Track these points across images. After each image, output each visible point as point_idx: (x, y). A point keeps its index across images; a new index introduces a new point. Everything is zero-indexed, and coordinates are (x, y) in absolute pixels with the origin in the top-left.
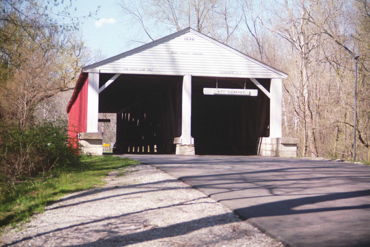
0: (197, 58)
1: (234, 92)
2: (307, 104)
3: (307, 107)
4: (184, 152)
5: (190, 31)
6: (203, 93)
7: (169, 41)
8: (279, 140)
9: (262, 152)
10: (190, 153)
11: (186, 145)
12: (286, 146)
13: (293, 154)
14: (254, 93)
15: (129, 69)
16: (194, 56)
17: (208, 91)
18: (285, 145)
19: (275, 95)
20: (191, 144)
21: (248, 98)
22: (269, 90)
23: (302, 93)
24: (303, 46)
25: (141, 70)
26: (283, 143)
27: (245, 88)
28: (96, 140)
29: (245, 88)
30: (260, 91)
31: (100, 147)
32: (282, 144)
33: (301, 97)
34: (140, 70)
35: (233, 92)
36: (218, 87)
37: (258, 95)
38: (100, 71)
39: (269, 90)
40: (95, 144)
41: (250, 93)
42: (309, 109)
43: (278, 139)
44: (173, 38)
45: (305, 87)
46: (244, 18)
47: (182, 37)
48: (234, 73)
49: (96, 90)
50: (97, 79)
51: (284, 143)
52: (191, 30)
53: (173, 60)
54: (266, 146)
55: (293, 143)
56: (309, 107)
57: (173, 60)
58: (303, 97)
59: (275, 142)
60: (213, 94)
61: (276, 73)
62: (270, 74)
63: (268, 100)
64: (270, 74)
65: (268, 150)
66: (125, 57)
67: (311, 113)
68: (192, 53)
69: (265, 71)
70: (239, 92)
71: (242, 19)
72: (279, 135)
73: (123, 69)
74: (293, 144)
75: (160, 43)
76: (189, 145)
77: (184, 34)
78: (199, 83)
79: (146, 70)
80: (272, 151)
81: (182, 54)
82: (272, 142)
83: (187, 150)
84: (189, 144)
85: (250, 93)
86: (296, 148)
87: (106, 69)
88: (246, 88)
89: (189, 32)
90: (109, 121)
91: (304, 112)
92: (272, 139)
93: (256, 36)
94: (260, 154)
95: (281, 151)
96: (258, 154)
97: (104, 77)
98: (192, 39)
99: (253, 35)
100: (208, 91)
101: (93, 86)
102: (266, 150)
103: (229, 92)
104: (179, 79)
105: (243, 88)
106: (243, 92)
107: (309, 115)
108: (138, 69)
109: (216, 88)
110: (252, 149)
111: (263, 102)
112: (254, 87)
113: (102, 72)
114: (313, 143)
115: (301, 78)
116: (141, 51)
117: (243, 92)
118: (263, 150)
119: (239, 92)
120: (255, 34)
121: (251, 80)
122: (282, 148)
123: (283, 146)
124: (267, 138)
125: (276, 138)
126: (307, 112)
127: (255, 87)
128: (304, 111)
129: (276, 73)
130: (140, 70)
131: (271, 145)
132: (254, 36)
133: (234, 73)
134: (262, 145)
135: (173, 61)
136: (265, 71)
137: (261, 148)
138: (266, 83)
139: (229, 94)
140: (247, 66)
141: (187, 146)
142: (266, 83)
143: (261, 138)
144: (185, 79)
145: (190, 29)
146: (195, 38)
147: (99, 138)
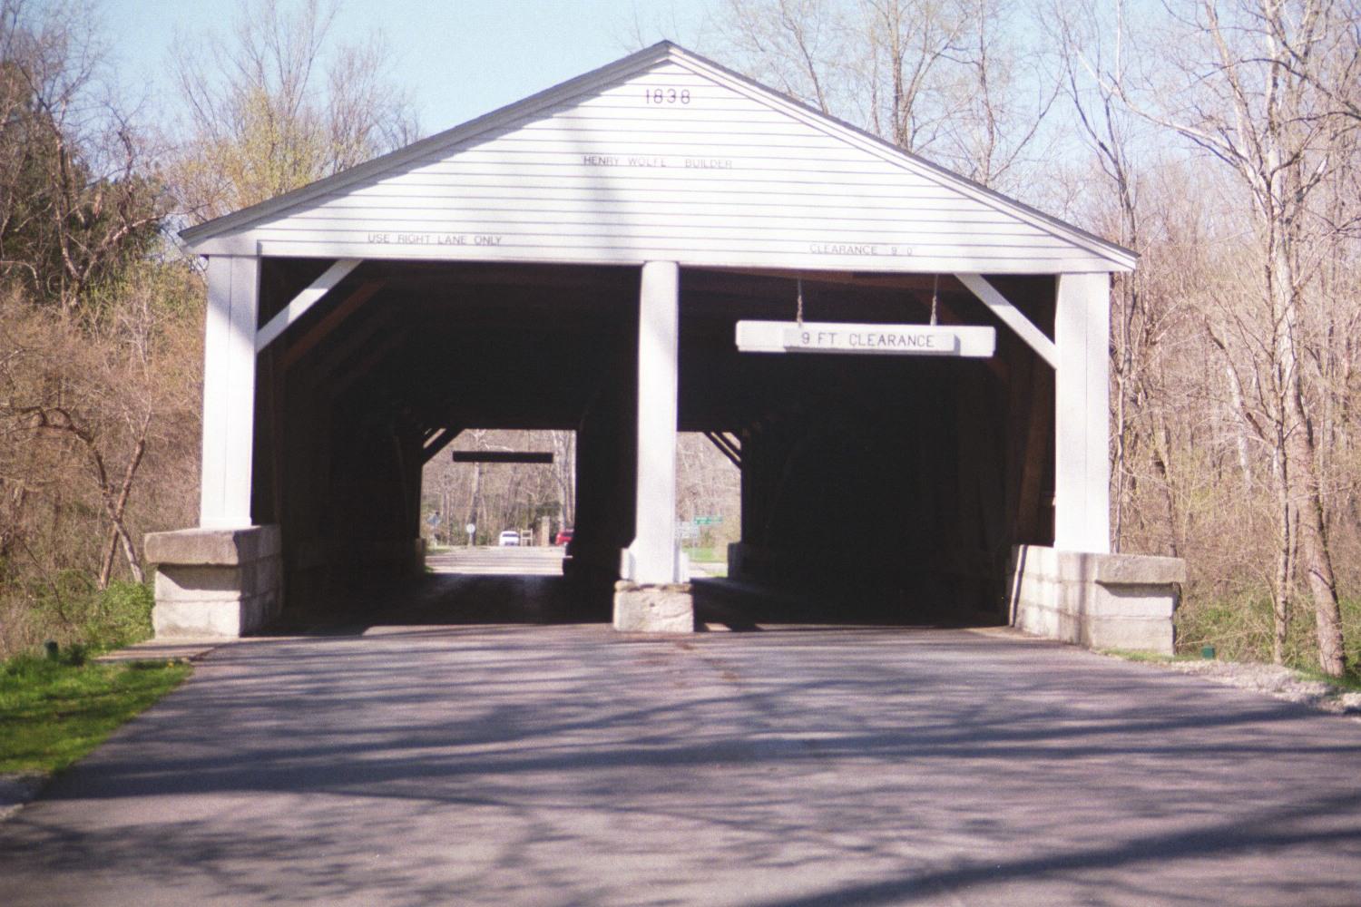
0: (705, 181)
1: (882, 339)
2: (1291, 392)
3: (1290, 404)
4: (642, 619)
5: (672, 58)
6: (735, 347)
7: (575, 106)
8: (1089, 565)
9: (1023, 611)
10: (669, 621)
11: (651, 586)
12: (1120, 595)
13: (1153, 634)
14: (977, 342)
15: (393, 238)
16: (692, 173)
17: (755, 336)
18: (1117, 588)
19: (1077, 356)
20: (676, 580)
21: (950, 364)
22: (1048, 329)
23: (1270, 350)
24: (1272, 174)
25: (448, 242)
26: (1105, 580)
27: (933, 318)
28: (207, 566)
29: (933, 318)
30: (1006, 336)
31: (228, 601)
32: (1098, 582)
33: (1268, 367)
34: (443, 240)
35: (875, 340)
36: (809, 317)
37: (996, 353)
38: (259, 246)
39: (1049, 331)
40: (203, 587)
41: (957, 342)
42: (1301, 412)
43: (1084, 559)
44: (594, 93)
45: (1283, 328)
46: (1069, 87)
47: (634, 88)
48: (879, 249)
49: (243, 330)
50: (246, 281)
51: (1112, 580)
52: (675, 55)
53: (600, 194)
54: (1041, 582)
55: (1152, 579)
56: (1299, 404)
57: (600, 194)
58: (1277, 367)
59: (1072, 573)
60: (783, 350)
61: (1079, 246)
62: (1054, 253)
63: (1041, 378)
64: (1054, 253)
65: (1049, 609)
66: (375, 183)
67: (1309, 424)
68: (681, 161)
69: (1032, 241)
70: (902, 340)
71: (1061, 90)
72: (1099, 543)
73: (364, 237)
74: (1153, 586)
75: (532, 117)
76: (664, 588)
77: (643, 72)
78: (714, 297)
79: (470, 239)
80: (1062, 612)
81: (632, 164)
82: (1060, 570)
83: (655, 610)
84: (667, 579)
85: (957, 342)
86: (1166, 603)
87: (290, 237)
88: (940, 322)
89: (668, 62)
90: (547, 458)
91: (1280, 423)
92: (1063, 558)
93: (1111, 150)
94: (1018, 620)
95: (1099, 619)
96: (1011, 620)
97: (280, 277)
98: (679, 94)
99: (1102, 145)
100: (755, 336)
101: (229, 312)
102: (1041, 607)
103: (854, 340)
104: (626, 280)
105: (927, 322)
106: (923, 341)
107: (1299, 433)
108: (434, 238)
109: (792, 318)
110: (986, 600)
111: (1022, 385)
112: (974, 313)
113: (272, 250)
114: (1315, 539)
115: (1265, 294)
116: (447, 157)
117: (923, 341)
118: (1030, 604)
119: (902, 340)
120: (1108, 144)
121: (961, 279)
122: (1102, 604)
123: (1104, 592)
124: (1046, 550)
125: (1076, 554)
126: (1294, 420)
127: (981, 315)
128: (1279, 418)
129: (1078, 250)
130: (443, 239)
131: (1057, 585)
132: (1106, 149)
133: (879, 249)
134: (1024, 579)
135: (602, 197)
136: (1032, 241)
137: (1023, 596)
138: (1036, 294)
139: (858, 347)
140: (945, 216)
141: (655, 591)
142: (1036, 294)
143: (1021, 547)
144: (647, 275)
145: (673, 50)
146: (693, 92)
147: (218, 561)
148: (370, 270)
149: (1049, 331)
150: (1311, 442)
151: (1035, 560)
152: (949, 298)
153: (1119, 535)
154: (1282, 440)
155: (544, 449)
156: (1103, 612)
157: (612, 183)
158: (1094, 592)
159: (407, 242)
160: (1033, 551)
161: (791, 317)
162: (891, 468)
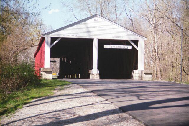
0: (100, 30)
3: (157, 55)
14: (130, 47)
15: (66, 35)
17: (106, 47)
19: (140, 49)
21: (127, 50)
28: (49, 71)
30: (133, 47)
36: (112, 45)
39: (137, 46)
40: (48, 73)
43: (142, 71)
46: (125, 9)
48: (120, 37)
49: (49, 46)
54: (136, 74)
59: (140, 72)
67: (159, 57)
68: (98, 27)
72: (143, 69)
76: (96, 74)
78: (102, 42)
79: (75, 36)
81: (93, 27)
84: (97, 73)
87: (54, 35)
90: (55, 62)
91: (155, 57)
92: (139, 71)
97: (53, 39)
100: (106, 47)
101: (48, 44)
102: (136, 77)
104: (91, 40)
108: (71, 35)
110: (128, 76)
111: (134, 52)
120: (130, 18)
122: (144, 75)
124: (136, 71)
126: (157, 57)
133: (120, 37)
135: (88, 31)
138: (136, 42)
142: (136, 42)
144: (94, 40)
146: (99, 20)
148: (63, 39)
149: (137, 46)
150: (159, 60)
151: (135, 72)
152: (127, 42)
153: (145, 69)
154: (156, 60)
155: (55, 60)
156: (145, 76)
157: (90, 29)
158: (143, 74)
159: (67, 36)
160: (135, 71)
161: (110, 45)
162: (119, 62)
